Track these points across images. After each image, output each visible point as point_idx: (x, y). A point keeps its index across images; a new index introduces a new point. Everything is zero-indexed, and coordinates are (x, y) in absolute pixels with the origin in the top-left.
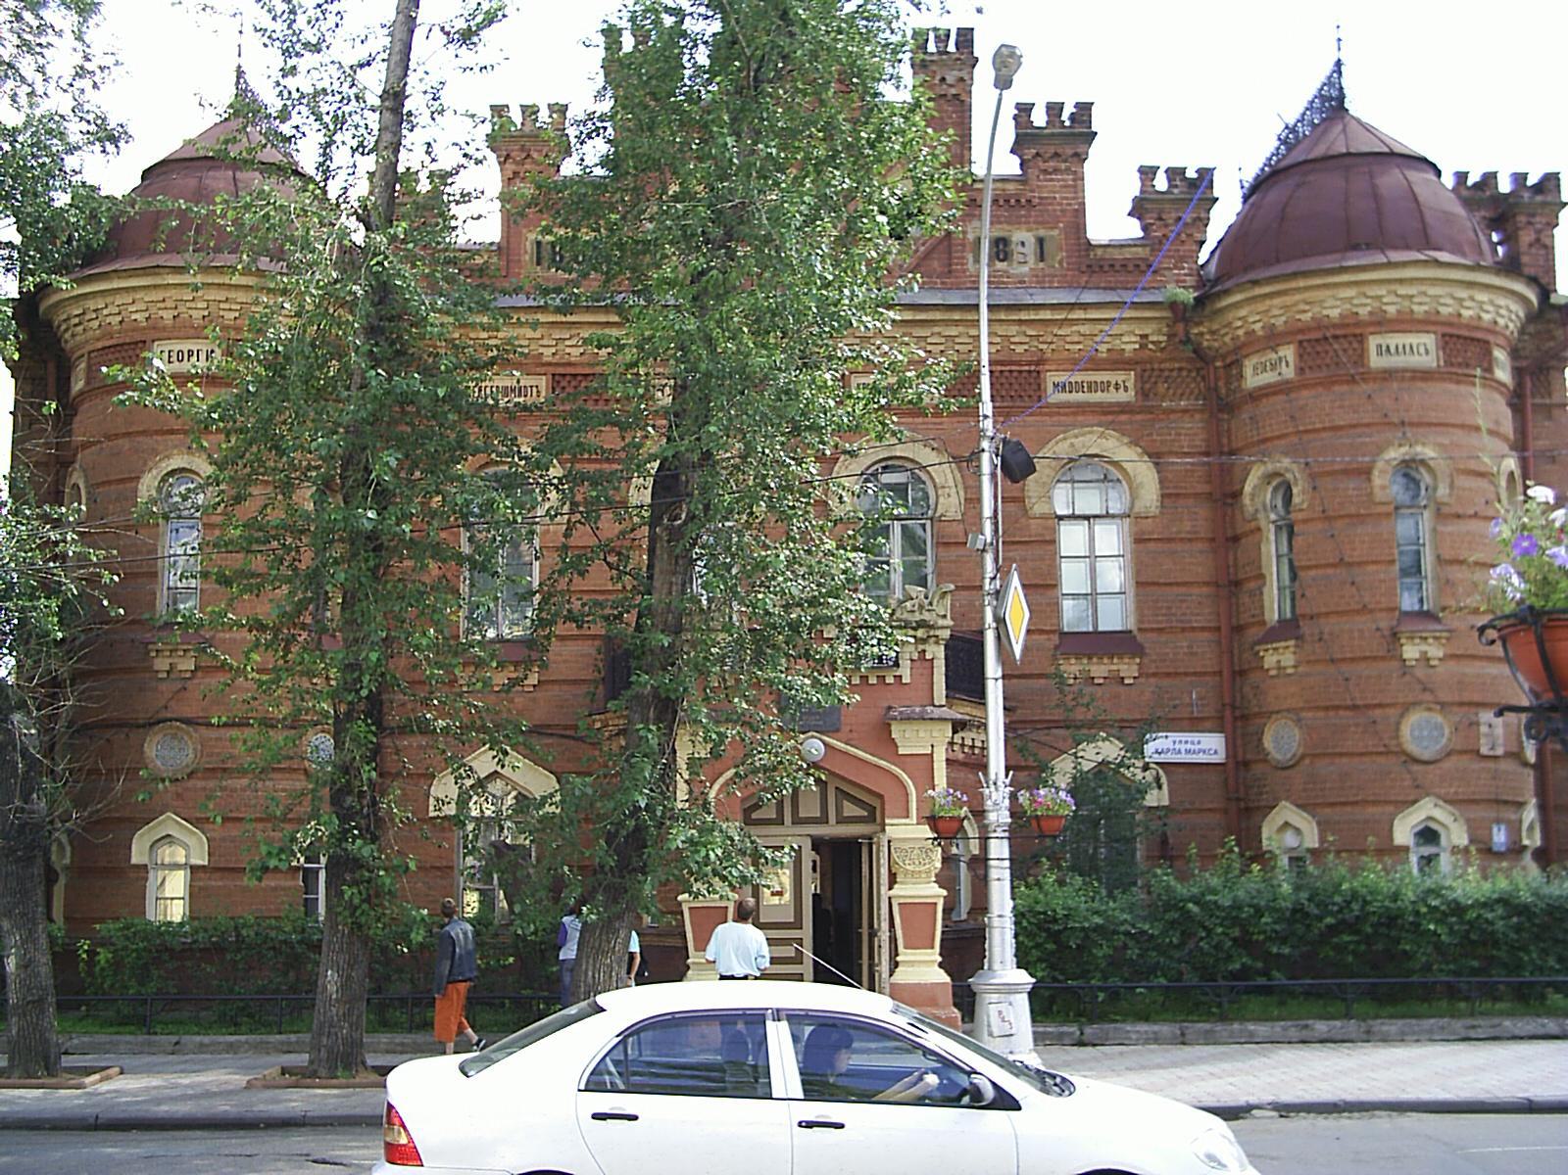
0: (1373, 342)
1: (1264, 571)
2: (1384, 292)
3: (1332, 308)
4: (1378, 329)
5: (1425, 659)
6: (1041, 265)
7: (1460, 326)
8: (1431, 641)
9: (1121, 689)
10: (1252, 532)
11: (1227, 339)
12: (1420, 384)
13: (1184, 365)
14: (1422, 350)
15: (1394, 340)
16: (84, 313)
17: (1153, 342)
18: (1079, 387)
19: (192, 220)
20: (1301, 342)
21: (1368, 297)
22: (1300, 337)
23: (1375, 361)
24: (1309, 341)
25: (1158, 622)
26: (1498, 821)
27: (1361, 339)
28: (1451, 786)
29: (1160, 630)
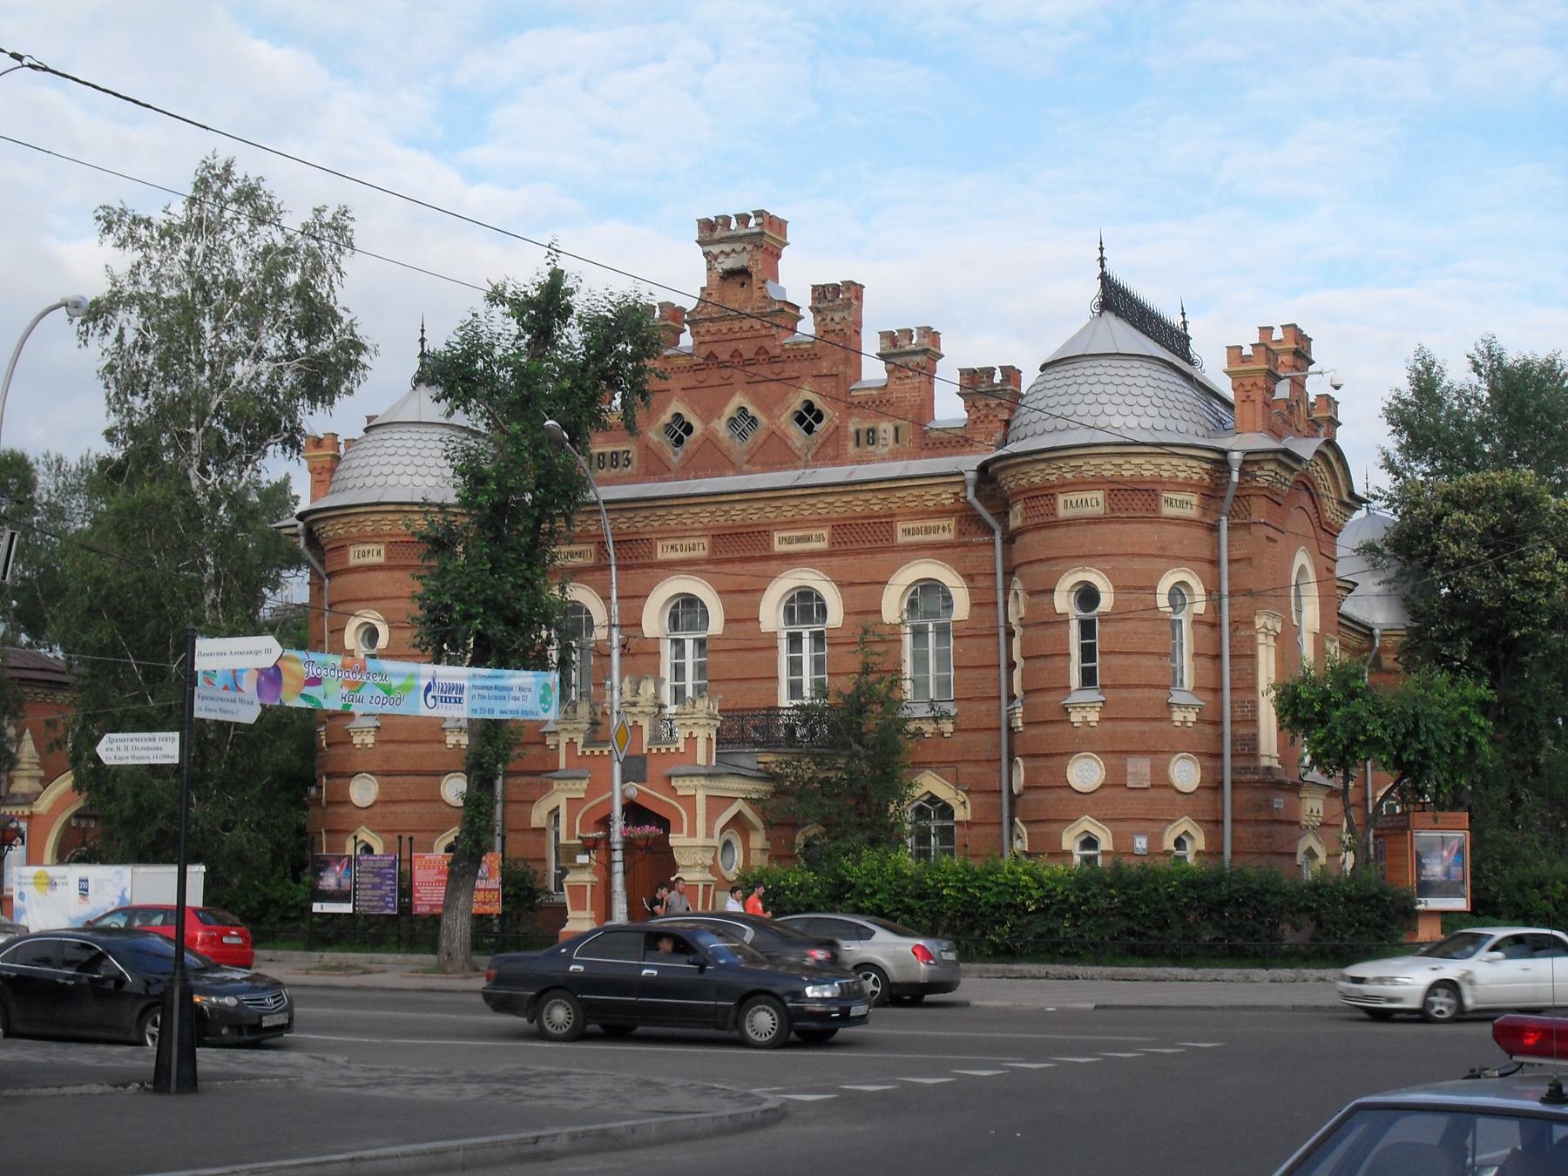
0: (1061, 499)
5: (1086, 723)
7: (1125, 483)
9: (941, 740)
10: (1061, 622)
12: (1093, 527)
14: (1094, 502)
15: (1074, 497)
18: (918, 531)
19: (93, 664)
23: (1062, 512)
26: (1141, 834)
29: (969, 699)
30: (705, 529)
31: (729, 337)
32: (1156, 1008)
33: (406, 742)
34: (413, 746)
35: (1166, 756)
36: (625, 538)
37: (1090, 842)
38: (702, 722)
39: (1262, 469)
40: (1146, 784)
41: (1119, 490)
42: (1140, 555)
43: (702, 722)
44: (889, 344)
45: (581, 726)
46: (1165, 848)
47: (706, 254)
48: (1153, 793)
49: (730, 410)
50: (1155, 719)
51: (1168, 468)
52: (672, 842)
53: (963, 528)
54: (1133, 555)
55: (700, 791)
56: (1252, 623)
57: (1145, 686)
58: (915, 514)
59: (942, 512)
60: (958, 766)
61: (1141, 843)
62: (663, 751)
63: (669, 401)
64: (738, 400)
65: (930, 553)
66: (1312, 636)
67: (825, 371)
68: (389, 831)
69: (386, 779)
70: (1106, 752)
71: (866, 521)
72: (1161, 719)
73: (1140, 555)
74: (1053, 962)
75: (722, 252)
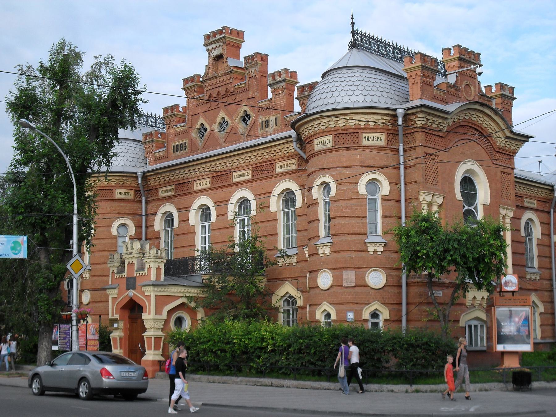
1: (196, 244)
6: (277, 127)
9: (293, 267)
16: (185, 172)
18: (284, 166)
25: (302, 243)
28: (332, 298)
30: (209, 174)
31: (217, 86)
32: (266, 409)
33: (101, 276)
34: (104, 278)
35: (364, 270)
36: (183, 181)
37: (328, 316)
38: (152, 260)
39: (417, 117)
40: (353, 285)
41: (338, 134)
42: (350, 167)
43: (152, 260)
44: (272, 79)
45: (115, 264)
46: (363, 318)
47: (208, 50)
48: (357, 289)
49: (219, 120)
50: (358, 251)
51: (362, 120)
52: (143, 317)
53: (300, 163)
54: (347, 167)
55: (152, 292)
56: (417, 199)
57: (353, 234)
59: (291, 156)
60: (299, 279)
61: (350, 316)
62: (141, 274)
63: (198, 118)
64: (222, 114)
65: (288, 176)
66: (482, 206)
67: (250, 96)
68: (94, 315)
69: (93, 292)
70: (334, 269)
71: (264, 164)
73: (350, 167)
74: (278, 377)
75: (213, 48)
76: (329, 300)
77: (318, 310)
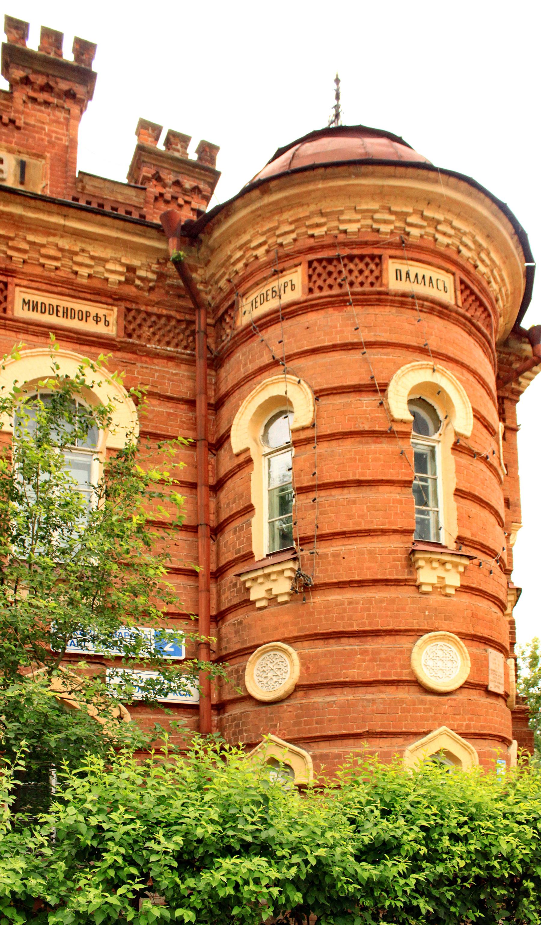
2: (410, 210)
3: (350, 221)
4: (398, 253)
8: (449, 566)
11: (222, 283)
13: (173, 313)
17: (141, 278)
20: (310, 263)
21: (391, 212)
22: (311, 257)
24: (320, 261)
27: (377, 259)
58: (51, 282)
72: (397, 582)
76: (456, 723)
77: (412, 751)
